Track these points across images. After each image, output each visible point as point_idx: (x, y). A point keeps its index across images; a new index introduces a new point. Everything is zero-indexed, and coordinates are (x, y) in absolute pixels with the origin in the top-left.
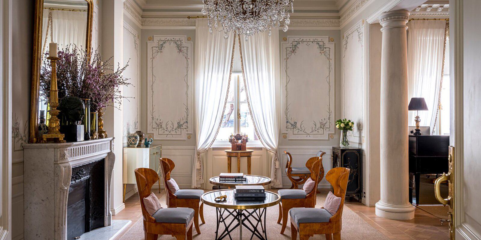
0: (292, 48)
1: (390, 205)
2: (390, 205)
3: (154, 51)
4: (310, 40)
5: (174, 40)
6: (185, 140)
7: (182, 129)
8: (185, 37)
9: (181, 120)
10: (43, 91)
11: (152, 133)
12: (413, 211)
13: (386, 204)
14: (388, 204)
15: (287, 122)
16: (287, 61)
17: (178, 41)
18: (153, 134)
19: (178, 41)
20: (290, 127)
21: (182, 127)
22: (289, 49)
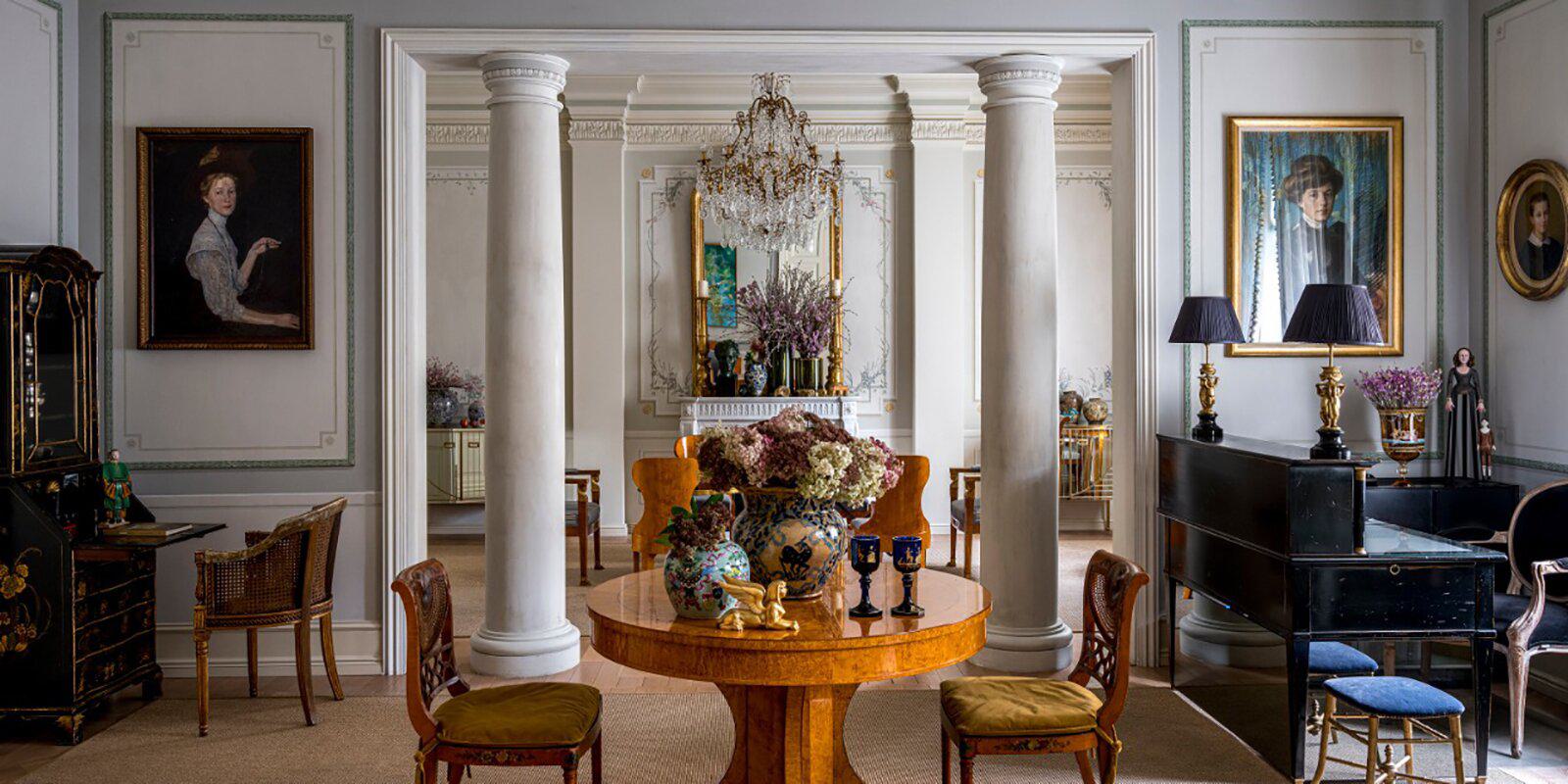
0: (664, 196)
1: (1217, 624)
2: (1217, 624)
3: (655, 203)
4: (475, 175)
5: (852, 176)
6: (880, 415)
7: (872, 390)
8: (879, 170)
9: (870, 366)
10: (827, 295)
11: (652, 398)
12: (575, 644)
13: (1210, 621)
14: (1214, 619)
15: (653, 374)
16: (652, 226)
17: (1105, 179)
18: (654, 402)
19: (1105, 179)
20: (661, 385)
21: (872, 384)
22: (659, 197)
